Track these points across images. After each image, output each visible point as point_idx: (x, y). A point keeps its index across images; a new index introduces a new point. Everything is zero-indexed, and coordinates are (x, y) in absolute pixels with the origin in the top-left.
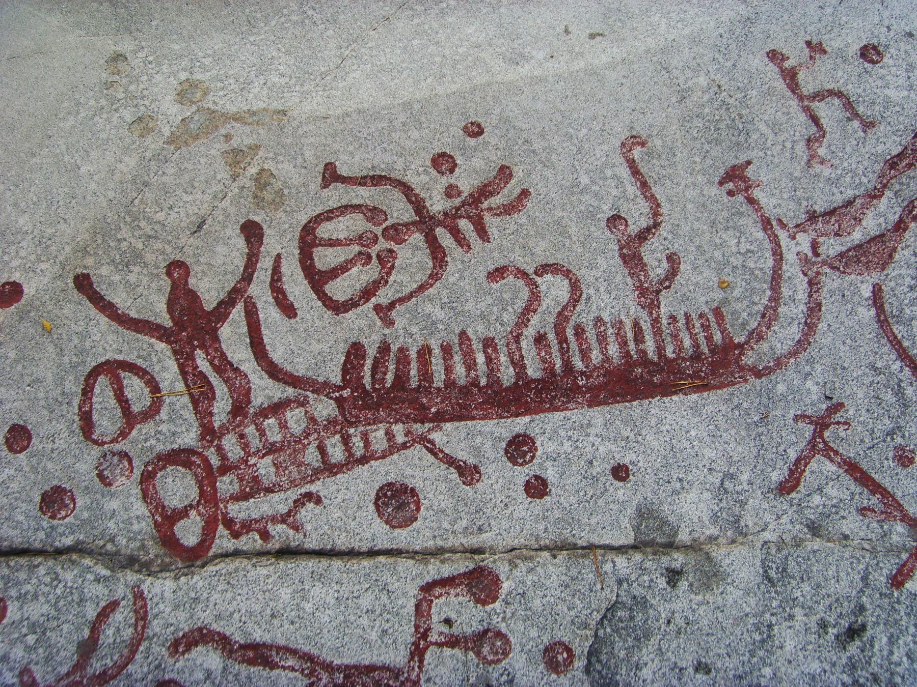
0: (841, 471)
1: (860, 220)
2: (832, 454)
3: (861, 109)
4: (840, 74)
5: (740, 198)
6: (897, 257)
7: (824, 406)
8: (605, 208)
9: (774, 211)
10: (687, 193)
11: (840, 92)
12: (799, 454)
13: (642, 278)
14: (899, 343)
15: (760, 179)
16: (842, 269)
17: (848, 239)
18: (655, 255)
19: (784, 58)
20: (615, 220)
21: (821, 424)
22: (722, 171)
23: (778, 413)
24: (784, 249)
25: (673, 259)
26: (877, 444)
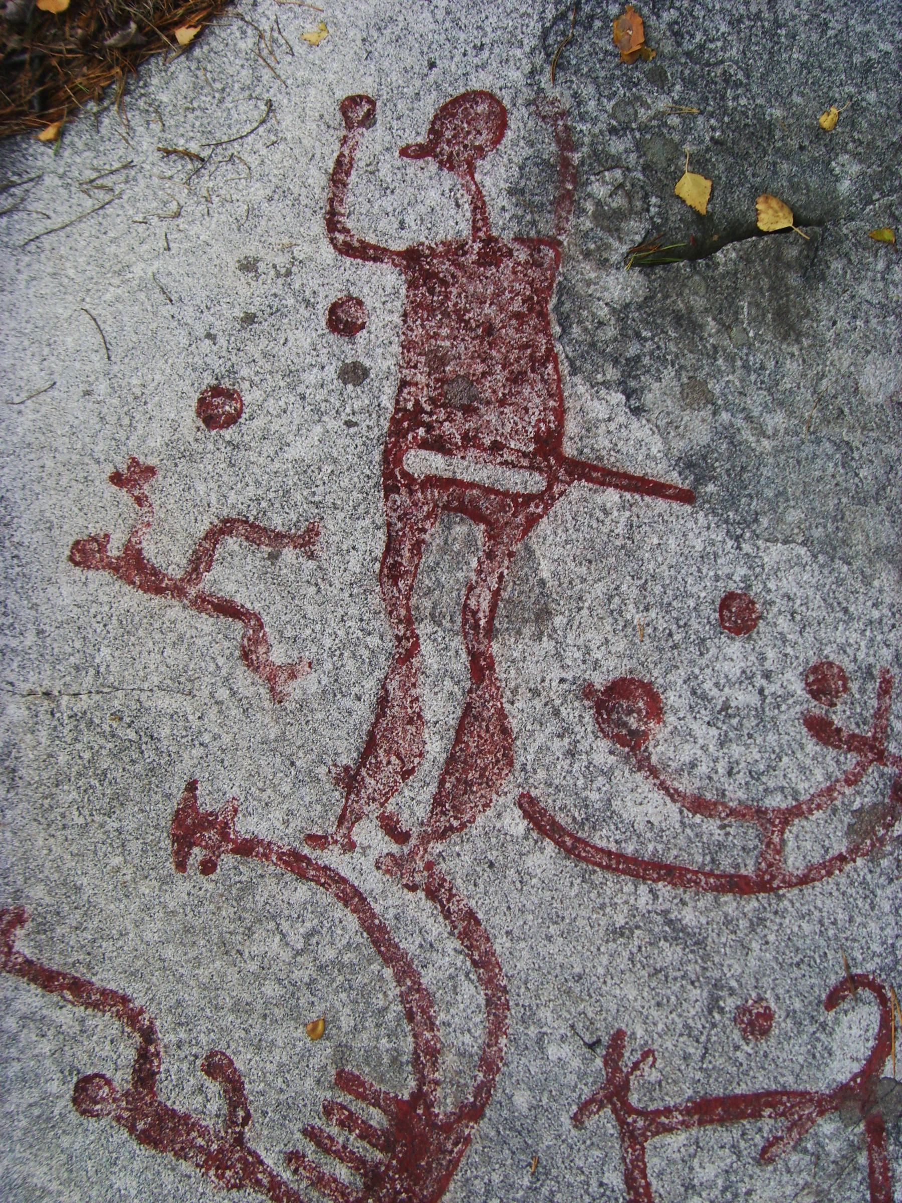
0: (694, 1131)
1: (420, 717)
2: (663, 1119)
3: (277, 522)
4: (201, 488)
5: (228, 861)
6: (514, 724)
7: (599, 1062)
8: (54, 1087)
9: (289, 831)
10: (148, 936)
11: (225, 521)
12: (622, 1167)
13: (200, 1141)
14: (620, 857)
15: (229, 796)
16: (456, 823)
17: (426, 766)
18: (188, 1088)
19: (102, 542)
20: (85, 1092)
21: (614, 1093)
22: (166, 843)
23: (548, 1140)
24: (352, 877)
25: (217, 1066)
26: (708, 1040)
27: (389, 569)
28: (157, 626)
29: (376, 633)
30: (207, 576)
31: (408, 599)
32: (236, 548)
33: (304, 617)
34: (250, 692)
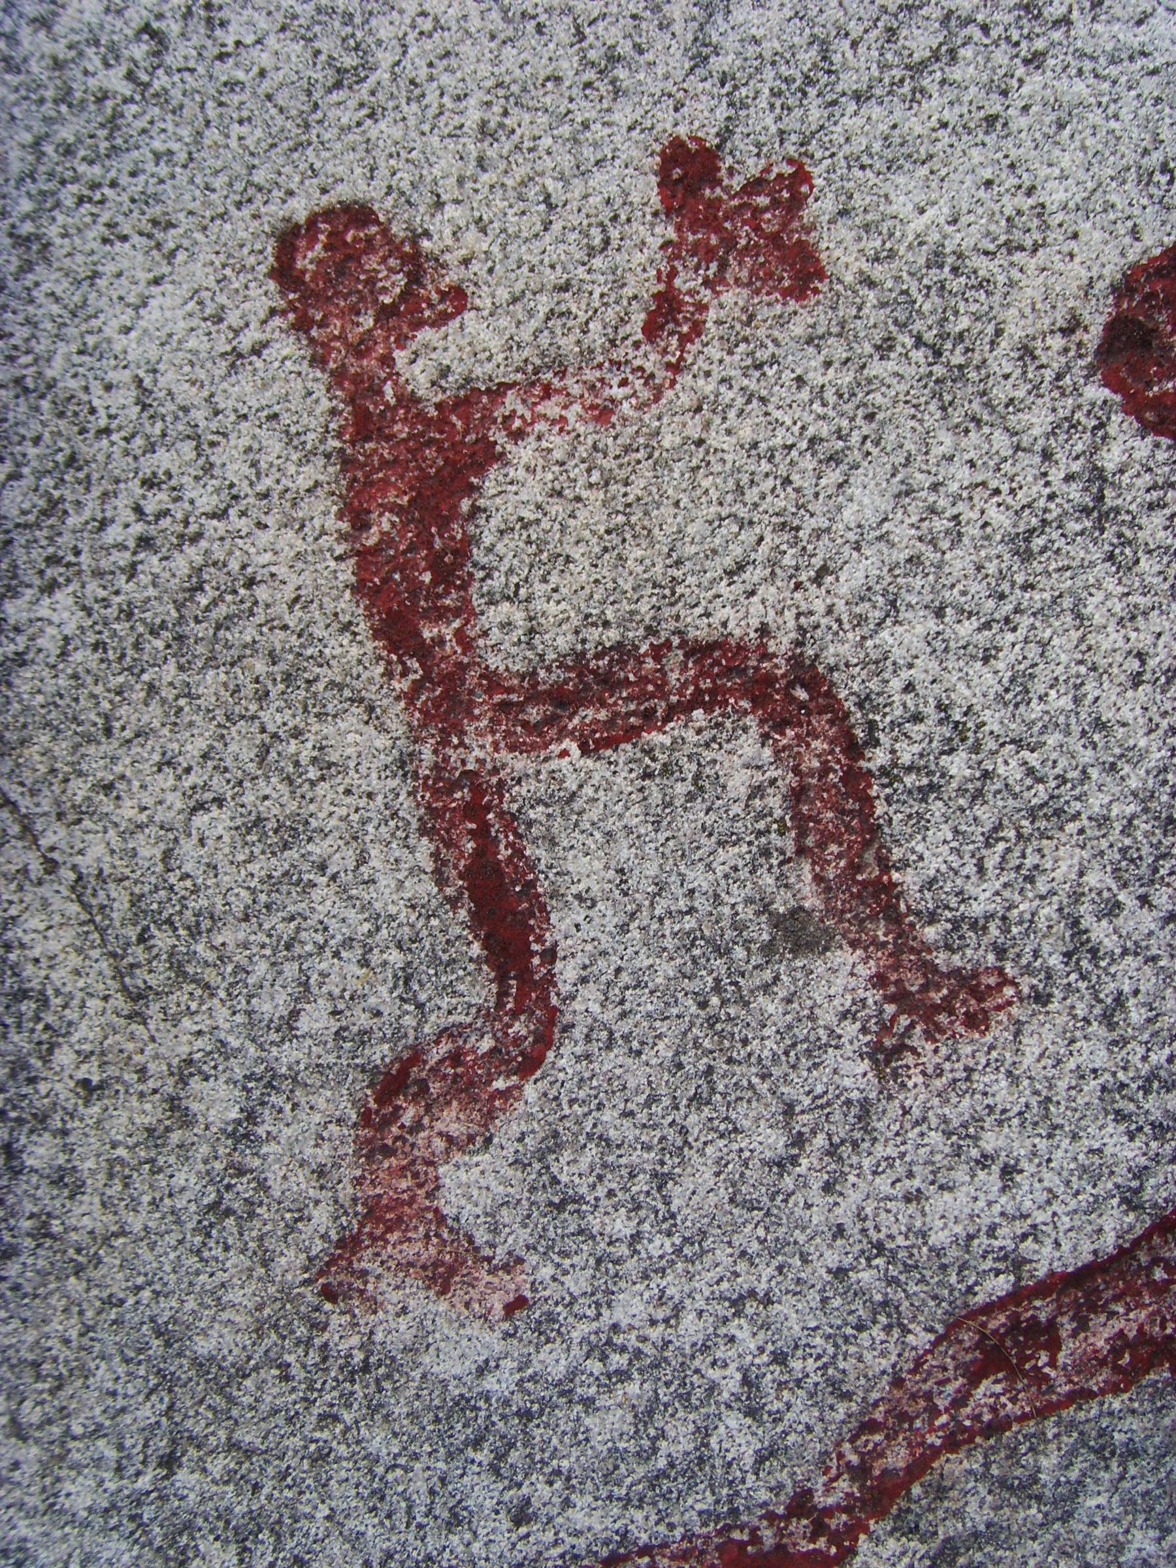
3: (926, 854)
4: (867, 499)
11: (806, 673)
19: (426, 296)
27: (1014, 1325)
28: (272, 718)
29: (768, 1433)
30: (569, 762)
31: (952, 1444)
32: (739, 783)
33: (661, 1180)
34: (288, 1181)
